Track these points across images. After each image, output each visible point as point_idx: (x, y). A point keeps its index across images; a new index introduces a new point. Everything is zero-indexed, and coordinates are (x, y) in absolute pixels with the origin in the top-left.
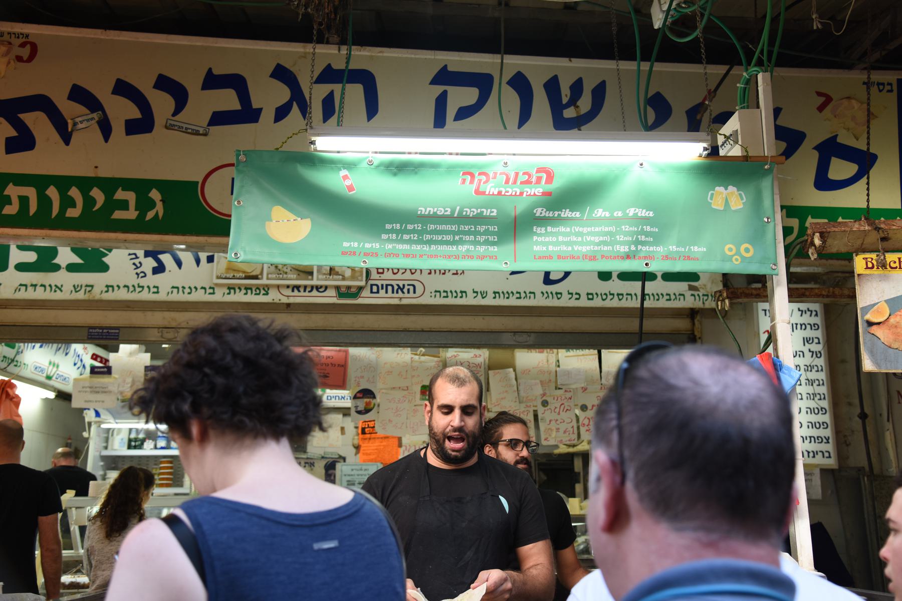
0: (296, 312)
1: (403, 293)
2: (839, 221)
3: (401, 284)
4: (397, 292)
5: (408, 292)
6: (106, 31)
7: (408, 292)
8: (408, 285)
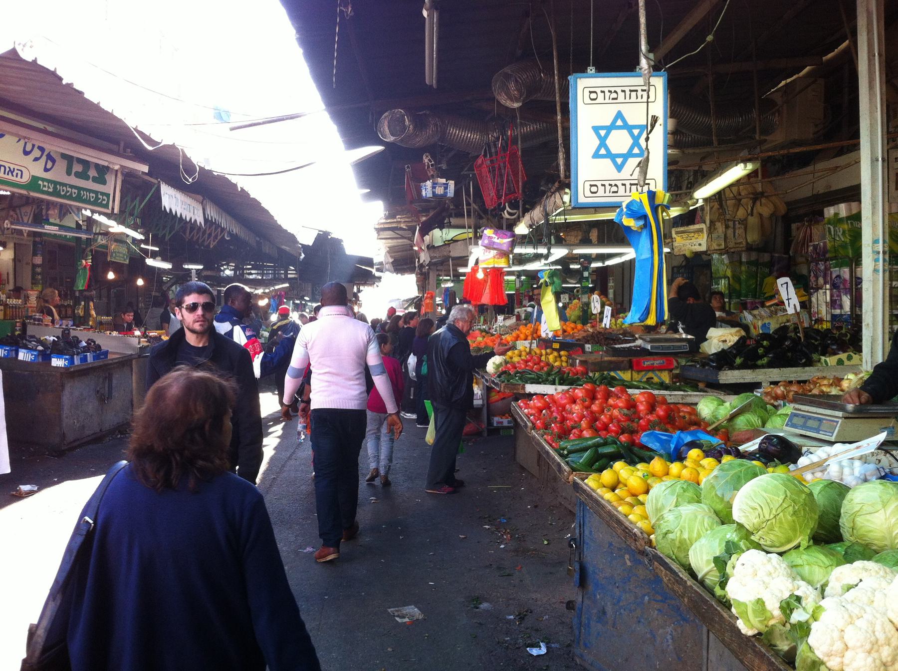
0: (819, 416)
1: (13, 176)
2: (82, 314)
3: (12, 167)
4: (8, 174)
5: (17, 176)
6: (35, 61)
7: (17, 176)
8: (17, 170)
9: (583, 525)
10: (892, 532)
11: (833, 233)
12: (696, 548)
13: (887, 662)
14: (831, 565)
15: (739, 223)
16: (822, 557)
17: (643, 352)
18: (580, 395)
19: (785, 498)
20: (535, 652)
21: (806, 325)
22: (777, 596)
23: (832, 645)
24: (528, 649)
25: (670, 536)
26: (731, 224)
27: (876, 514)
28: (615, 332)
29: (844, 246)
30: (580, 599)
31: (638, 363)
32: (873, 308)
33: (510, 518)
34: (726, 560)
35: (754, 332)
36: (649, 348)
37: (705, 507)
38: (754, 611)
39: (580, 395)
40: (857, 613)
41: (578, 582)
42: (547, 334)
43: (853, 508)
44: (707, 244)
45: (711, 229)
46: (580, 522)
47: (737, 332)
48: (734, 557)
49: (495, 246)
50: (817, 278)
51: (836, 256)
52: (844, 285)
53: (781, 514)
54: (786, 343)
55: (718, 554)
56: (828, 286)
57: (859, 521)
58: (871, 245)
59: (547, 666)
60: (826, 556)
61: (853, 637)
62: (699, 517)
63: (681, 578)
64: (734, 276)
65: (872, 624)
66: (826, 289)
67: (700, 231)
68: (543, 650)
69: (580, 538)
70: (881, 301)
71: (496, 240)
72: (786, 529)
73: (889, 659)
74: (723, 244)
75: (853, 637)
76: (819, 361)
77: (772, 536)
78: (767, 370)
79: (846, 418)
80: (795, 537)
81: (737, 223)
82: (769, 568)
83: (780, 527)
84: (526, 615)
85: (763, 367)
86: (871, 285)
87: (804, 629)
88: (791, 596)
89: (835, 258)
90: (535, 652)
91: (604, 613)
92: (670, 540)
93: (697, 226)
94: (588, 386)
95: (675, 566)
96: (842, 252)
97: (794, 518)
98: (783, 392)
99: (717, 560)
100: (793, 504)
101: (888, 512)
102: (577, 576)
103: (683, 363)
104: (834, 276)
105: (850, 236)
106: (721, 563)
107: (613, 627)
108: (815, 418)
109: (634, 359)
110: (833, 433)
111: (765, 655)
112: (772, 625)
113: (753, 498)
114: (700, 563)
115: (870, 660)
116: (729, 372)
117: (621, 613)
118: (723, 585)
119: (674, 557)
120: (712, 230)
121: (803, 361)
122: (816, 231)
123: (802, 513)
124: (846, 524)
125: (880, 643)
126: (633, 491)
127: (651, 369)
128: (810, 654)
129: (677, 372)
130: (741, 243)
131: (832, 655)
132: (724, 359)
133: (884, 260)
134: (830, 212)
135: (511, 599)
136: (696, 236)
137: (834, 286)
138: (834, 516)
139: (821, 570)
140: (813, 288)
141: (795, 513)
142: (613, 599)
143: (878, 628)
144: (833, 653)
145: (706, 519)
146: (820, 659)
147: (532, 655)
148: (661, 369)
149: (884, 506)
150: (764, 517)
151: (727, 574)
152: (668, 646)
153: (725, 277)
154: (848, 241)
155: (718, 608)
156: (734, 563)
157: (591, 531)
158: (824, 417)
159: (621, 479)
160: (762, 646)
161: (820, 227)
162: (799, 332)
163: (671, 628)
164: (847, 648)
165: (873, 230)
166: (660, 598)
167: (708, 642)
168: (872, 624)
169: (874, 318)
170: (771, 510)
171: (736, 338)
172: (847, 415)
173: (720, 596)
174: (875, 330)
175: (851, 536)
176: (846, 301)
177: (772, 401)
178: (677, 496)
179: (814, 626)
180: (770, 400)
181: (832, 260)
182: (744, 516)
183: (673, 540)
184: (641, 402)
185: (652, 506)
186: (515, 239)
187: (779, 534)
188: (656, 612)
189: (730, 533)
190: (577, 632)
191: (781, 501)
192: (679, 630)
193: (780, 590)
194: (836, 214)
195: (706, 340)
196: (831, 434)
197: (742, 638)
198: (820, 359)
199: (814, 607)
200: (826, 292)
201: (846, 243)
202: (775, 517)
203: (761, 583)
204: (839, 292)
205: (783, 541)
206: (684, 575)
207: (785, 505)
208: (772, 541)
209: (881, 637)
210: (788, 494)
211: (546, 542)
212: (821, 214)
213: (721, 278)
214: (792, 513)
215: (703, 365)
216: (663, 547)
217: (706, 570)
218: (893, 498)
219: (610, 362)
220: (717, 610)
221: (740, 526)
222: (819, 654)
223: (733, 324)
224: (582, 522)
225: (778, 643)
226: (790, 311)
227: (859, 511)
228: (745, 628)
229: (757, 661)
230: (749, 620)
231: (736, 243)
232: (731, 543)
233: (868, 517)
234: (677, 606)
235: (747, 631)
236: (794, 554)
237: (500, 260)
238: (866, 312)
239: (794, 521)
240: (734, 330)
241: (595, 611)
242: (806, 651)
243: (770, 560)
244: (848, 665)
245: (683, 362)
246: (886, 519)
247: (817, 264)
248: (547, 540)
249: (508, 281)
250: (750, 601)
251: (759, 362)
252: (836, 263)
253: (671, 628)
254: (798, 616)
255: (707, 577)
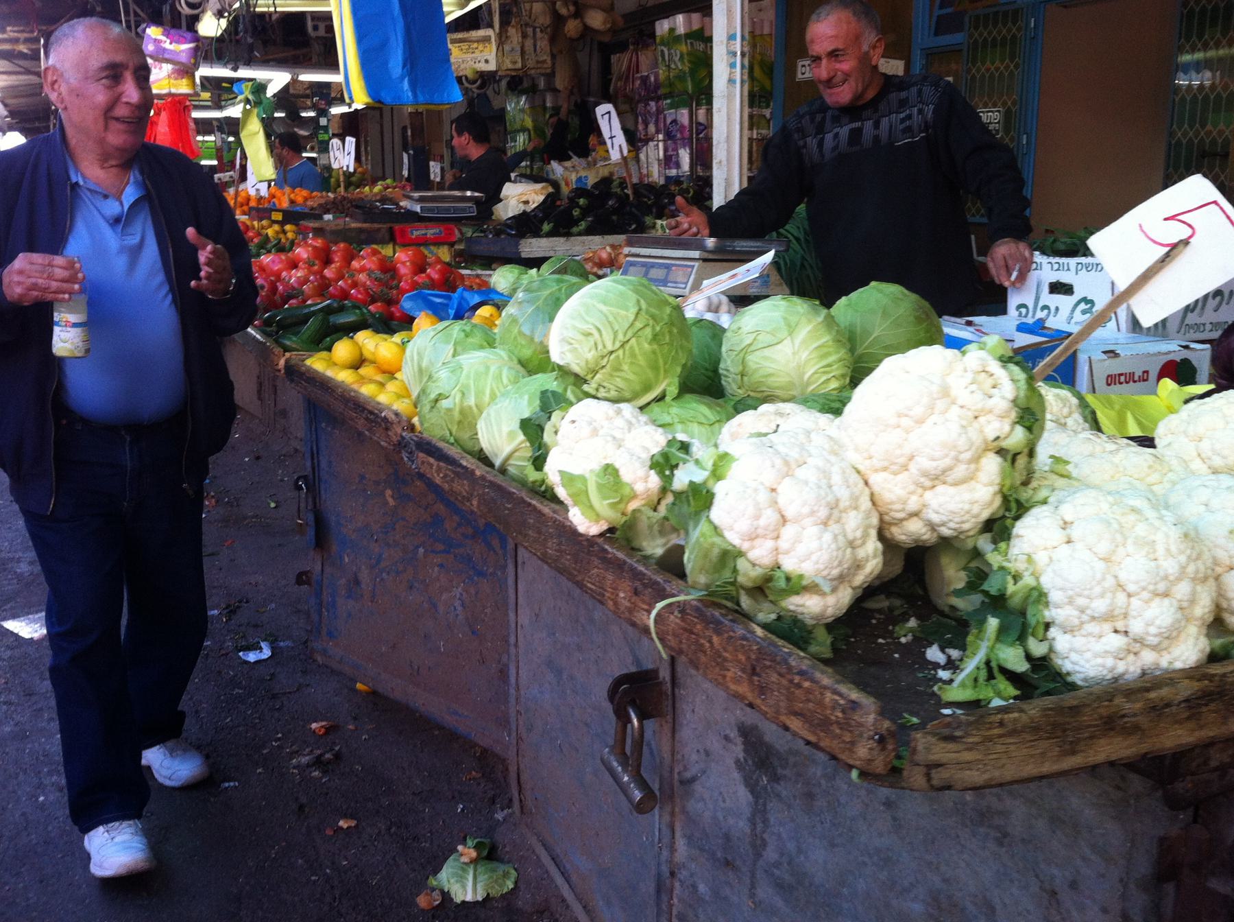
9: (318, 453)
10: (804, 373)
11: (667, 58)
12: (489, 414)
13: (855, 540)
14: (718, 421)
15: (541, 31)
16: (704, 409)
17: (411, 216)
18: (305, 256)
19: (638, 314)
20: (252, 657)
21: (635, 180)
22: (639, 458)
23: (757, 517)
24: (241, 654)
25: (444, 404)
26: (530, 31)
27: (779, 346)
28: (369, 198)
29: (681, 77)
30: (318, 567)
31: (403, 232)
32: (728, 137)
33: (215, 477)
34: (542, 423)
35: (565, 190)
36: (419, 210)
37: (503, 354)
38: (600, 487)
39: (305, 256)
40: (797, 456)
41: (314, 541)
42: (258, 190)
43: (741, 341)
44: (497, 61)
45: (502, 39)
46: (312, 448)
47: (543, 188)
48: (556, 416)
49: (166, 56)
50: (646, 124)
51: (670, 93)
52: (682, 133)
53: (633, 341)
54: (610, 203)
55: (526, 415)
56: (661, 137)
57: (753, 360)
58: (725, 42)
59: (273, 675)
60: (710, 407)
61: (793, 498)
62: (493, 369)
63: (465, 468)
64: (535, 128)
65: (826, 474)
66: (658, 141)
67: (486, 39)
68: (266, 653)
69: (314, 476)
70: (737, 127)
71: (167, 45)
72: (640, 366)
73: (859, 534)
74: (520, 60)
75: (793, 498)
76: (654, 227)
77: (618, 379)
78: (585, 238)
79: (705, 260)
80: (657, 382)
81: (538, 30)
82: (619, 422)
83: (632, 363)
84: (239, 607)
85: (580, 234)
86: (725, 101)
87: (701, 498)
88: (670, 443)
89: (669, 95)
90: (252, 657)
91: (357, 582)
92: (443, 411)
93: (481, 33)
94: (319, 243)
95: (454, 452)
96: (679, 86)
97: (655, 347)
98: (610, 254)
99: (525, 425)
100: (651, 322)
101: (797, 341)
102: (311, 533)
103: (469, 235)
104: (669, 120)
105: (690, 62)
106: (533, 429)
107: (372, 602)
108: (661, 266)
109: (397, 227)
110: (686, 283)
111: (625, 562)
112: (634, 511)
113: (584, 315)
114: (497, 436)
115: (828, 537)
116: (534, 241)
117: (382, 579)
118: (539, 462)
119: (452, 440)
120: (503, 39)
121: (633, 227)
122: (645, 59)
123: (667, 338)
124: (731, 370)
125: (842, 505)
126: (385, 367)
127: (423, 242)
128: (717, 540)
129: (462, 247)
130: (544, 62)
131: (757, 537)
132: (526, 224)
133: (743, 67)
134: (663, 27)
135: (215, 587)
136: (481, 47)
137: (669, 136)
138: (707, 370)
139: (703, 429)
140: (641, 140)
141: (655, 338)
142: (370, 559)
143: (836, 479)
144: (760, 531)
145: (505, 372)
146: (734, 546)
147: (247, 662)
148: (437, 242)
149: (790, 334)
150: (604, 347)
151: (545, 445)
152: (457, 615)
153: (524, 129)
154: (687, 69)
155: (534, 502)
156: (558, 425)
157: (330, 462)
158: (673, 262)
159: (367, 354)
160: (618, 549)
161: (650, 54)
162: (626, 187)
163: (460, 589)
164: (784, 520)
165: (728, 19)
166: (440, 547)
167: (517, 598)
168: (826, 474)
169: (729, 151)
170: (615, 334)
171: (541, 198)
172: (706, 255)
173: (534, 482)
174: (729, 170)
175: (739, 388)
176: (685, 157)
177: (595, 270)
178: (455, 344)
179: (719, 489)
180: (592, 268)
181: (666, 98)
182: (570, 351)
183: (449, 410)
184: (404, 263)
185: (413, 366)
186: (200, 44)
187: (631, 377)
188: (436, 569)
189: (548, 381)
190: (315, 617)
191: (632, 317)
192: (472, 591)
193: (644, 447)
194: (672, 30)
195: (501, 200)
196: (683, 286)
197: (580, 543)
198: (655, 224)
199: (715, 457)
200: (657, 145)
201: (685, 73)
202: (622, 346)
203: (609, 439)
204: (675, 143)
205: (638, 388)
206: (468, 462)
207: (639, 325)
208: (619, 390)
209: (843, 494)
210: (644, 306)
211: (273, 505)
212: (653, 35)
213: (519, 131)
214: (650, 336)
215: (498, 233)
216: (432, 426)
217: (507, 450)
218: (804, 319)
219: (361, 230)
220: (530, 504)
221: (562, 369)
222: (734, 538)
223: (535, 178)
224: (315, 448)
225: (645, 544)
226: (615, 156)
227: (750, 345)
228: (583, 522)
229: (610, 577)
230: (591, 507)
231: (538, 62)
232: (550, 395)
233: (767, 352)
234: (468, 555)
235: (589, 527)
236: (656, 408)
237: (179, 82)
238: (719, 143)
239: (654, 352)
240: (539, 186)
241: (343, 581)
242: (708, 533)
243: (619, 412)
244: (787, 552)
245: (469, 232)
246: (794, 354)
247: (647, 104)
248: (275, 502)
249: (211, 159)
250: (591, 471)
251: (575, 230)
252: (671, 104)
253: (460, 589)
254: (683, 478)
255: (511, 462)
